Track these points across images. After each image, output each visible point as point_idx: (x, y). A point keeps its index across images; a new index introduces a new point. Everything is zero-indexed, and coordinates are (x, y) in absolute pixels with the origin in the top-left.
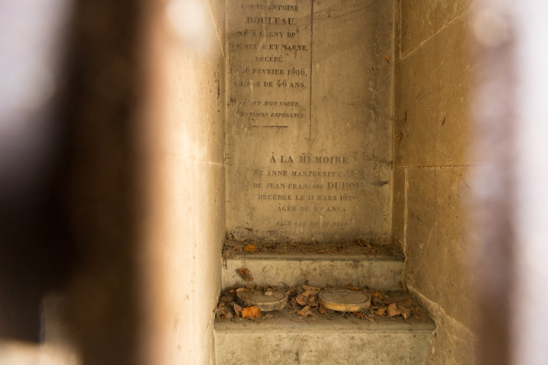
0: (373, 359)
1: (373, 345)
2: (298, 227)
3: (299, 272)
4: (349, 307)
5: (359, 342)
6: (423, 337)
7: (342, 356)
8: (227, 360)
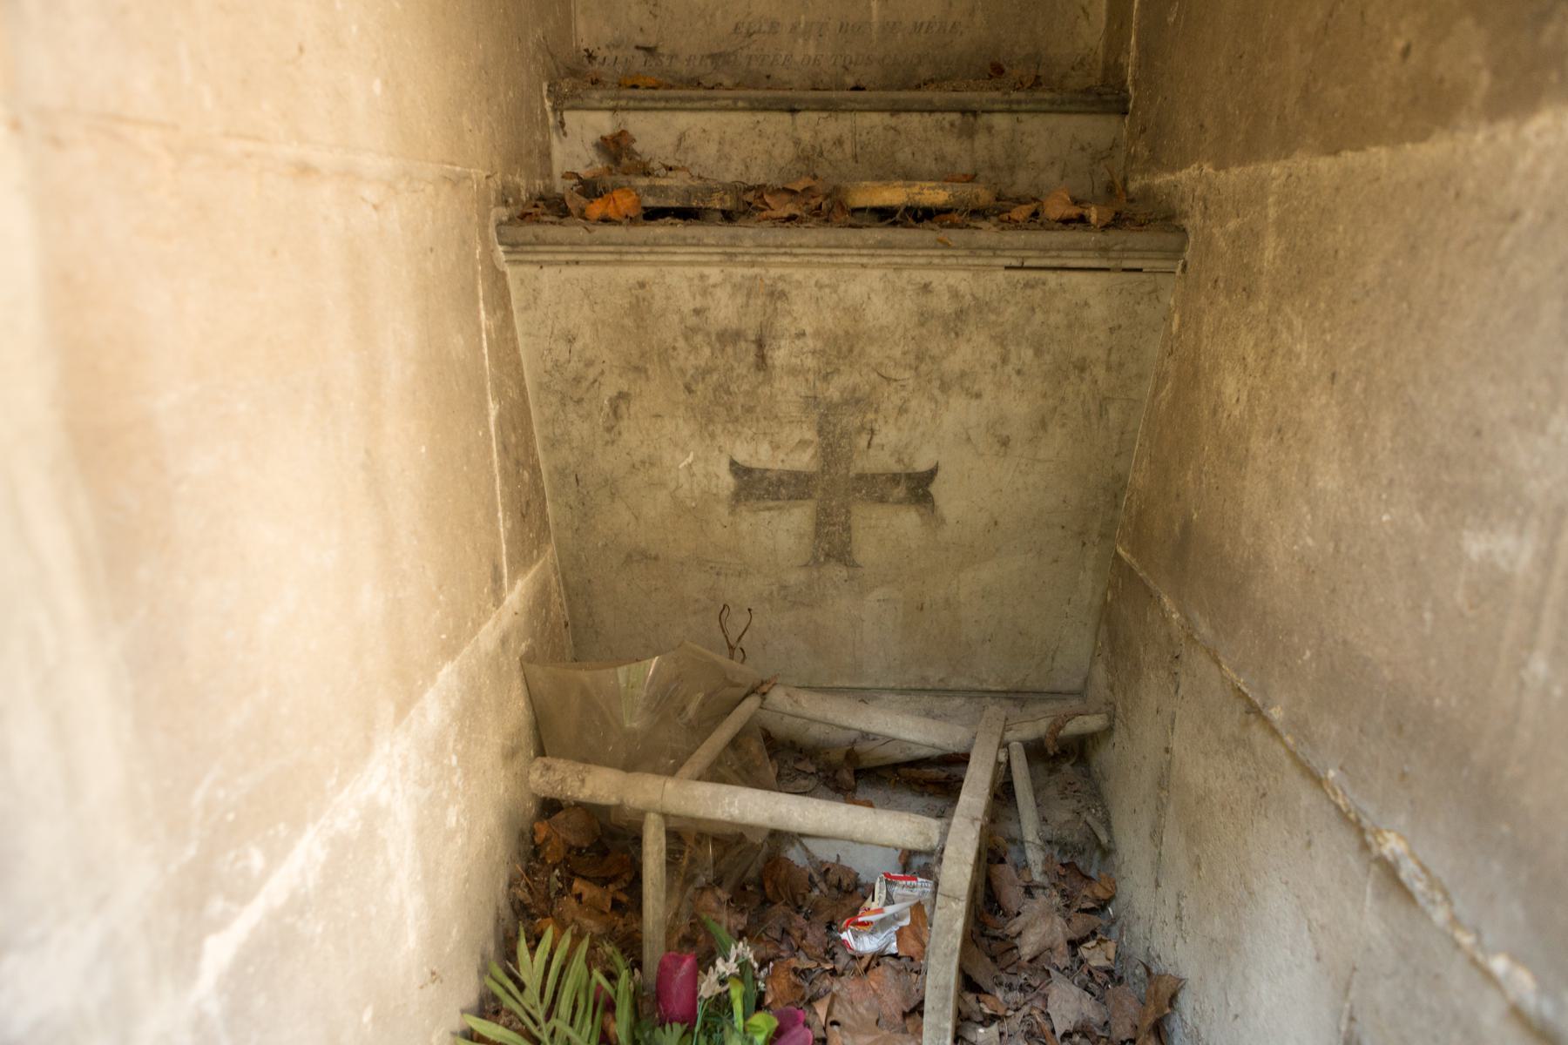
0: (994, 367)
1: (992, 317)
2: (801, 41)
3: (790, 151)
4: (916, 190)
5: (942, 303)
6: (1148, 288)
7: (897, 353)
8: (556, 364)
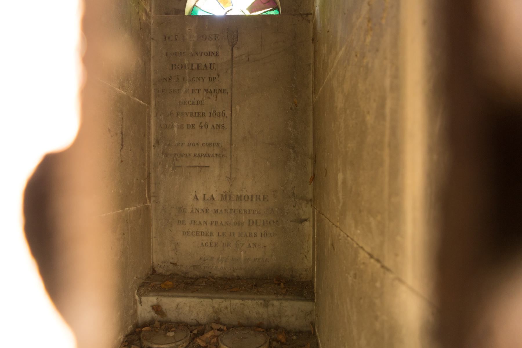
3: (211, 310)
